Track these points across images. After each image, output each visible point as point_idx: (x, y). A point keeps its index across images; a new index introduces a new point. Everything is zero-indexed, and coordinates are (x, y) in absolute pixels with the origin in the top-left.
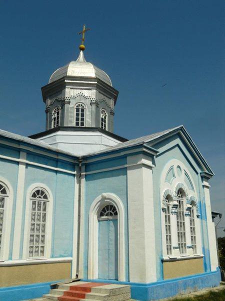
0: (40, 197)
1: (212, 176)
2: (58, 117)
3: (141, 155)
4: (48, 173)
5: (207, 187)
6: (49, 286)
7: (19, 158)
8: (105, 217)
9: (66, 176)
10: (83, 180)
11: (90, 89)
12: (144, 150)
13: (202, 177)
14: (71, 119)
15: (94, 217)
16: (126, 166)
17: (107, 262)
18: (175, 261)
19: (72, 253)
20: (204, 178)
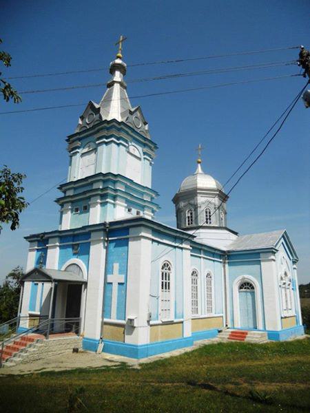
2: (191, 217)
3: (271, 254)
8: (243, 290)
10: (227, 265)
14: (202, 220)
15: (236, 288)
16: (128, 236)
19: (102, 327)
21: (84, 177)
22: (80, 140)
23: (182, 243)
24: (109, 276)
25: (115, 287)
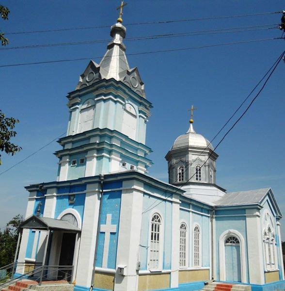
2: (183, 173)
5: (279, 225)
8: (229, 244)
10: (214, 220)
13: (277, 218)
15: (222, 243)
17: (232, 271)
18: (160, 274)
20: (278, 219)
22: (80, 96)
24: (102, 226)
25: (107, 236)
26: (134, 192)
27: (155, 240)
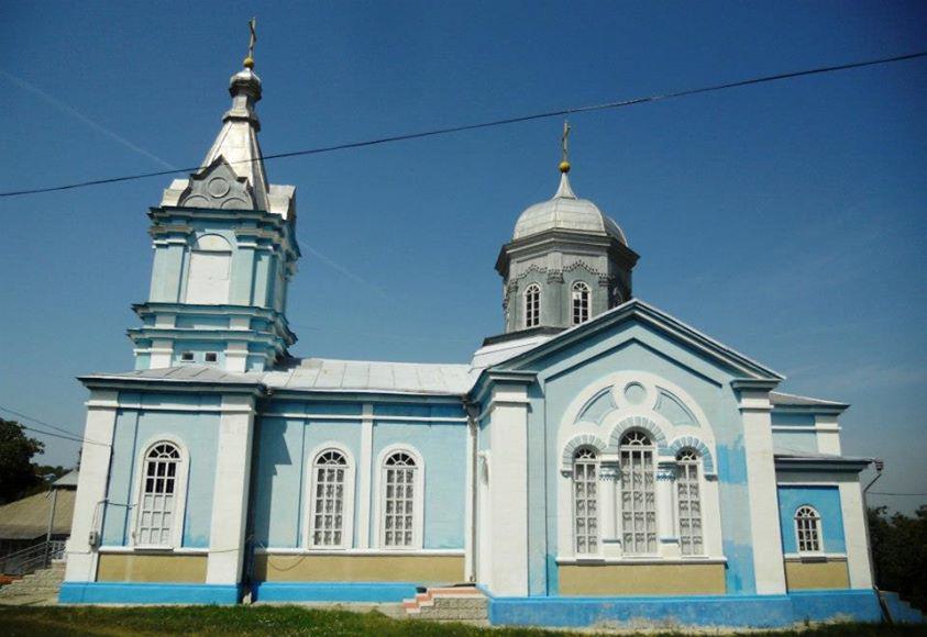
0: (636, 443)
1: (776, 383)
2: (585, 304)
4: (414, 427)
6: (414, 588)
7: (361, 414)
9: (451, 427)
11: (546, 254)
12: (492, 378)
21: (217, 304)
23: (219, 403)
26: (146, 414)
27: (158, 490)
